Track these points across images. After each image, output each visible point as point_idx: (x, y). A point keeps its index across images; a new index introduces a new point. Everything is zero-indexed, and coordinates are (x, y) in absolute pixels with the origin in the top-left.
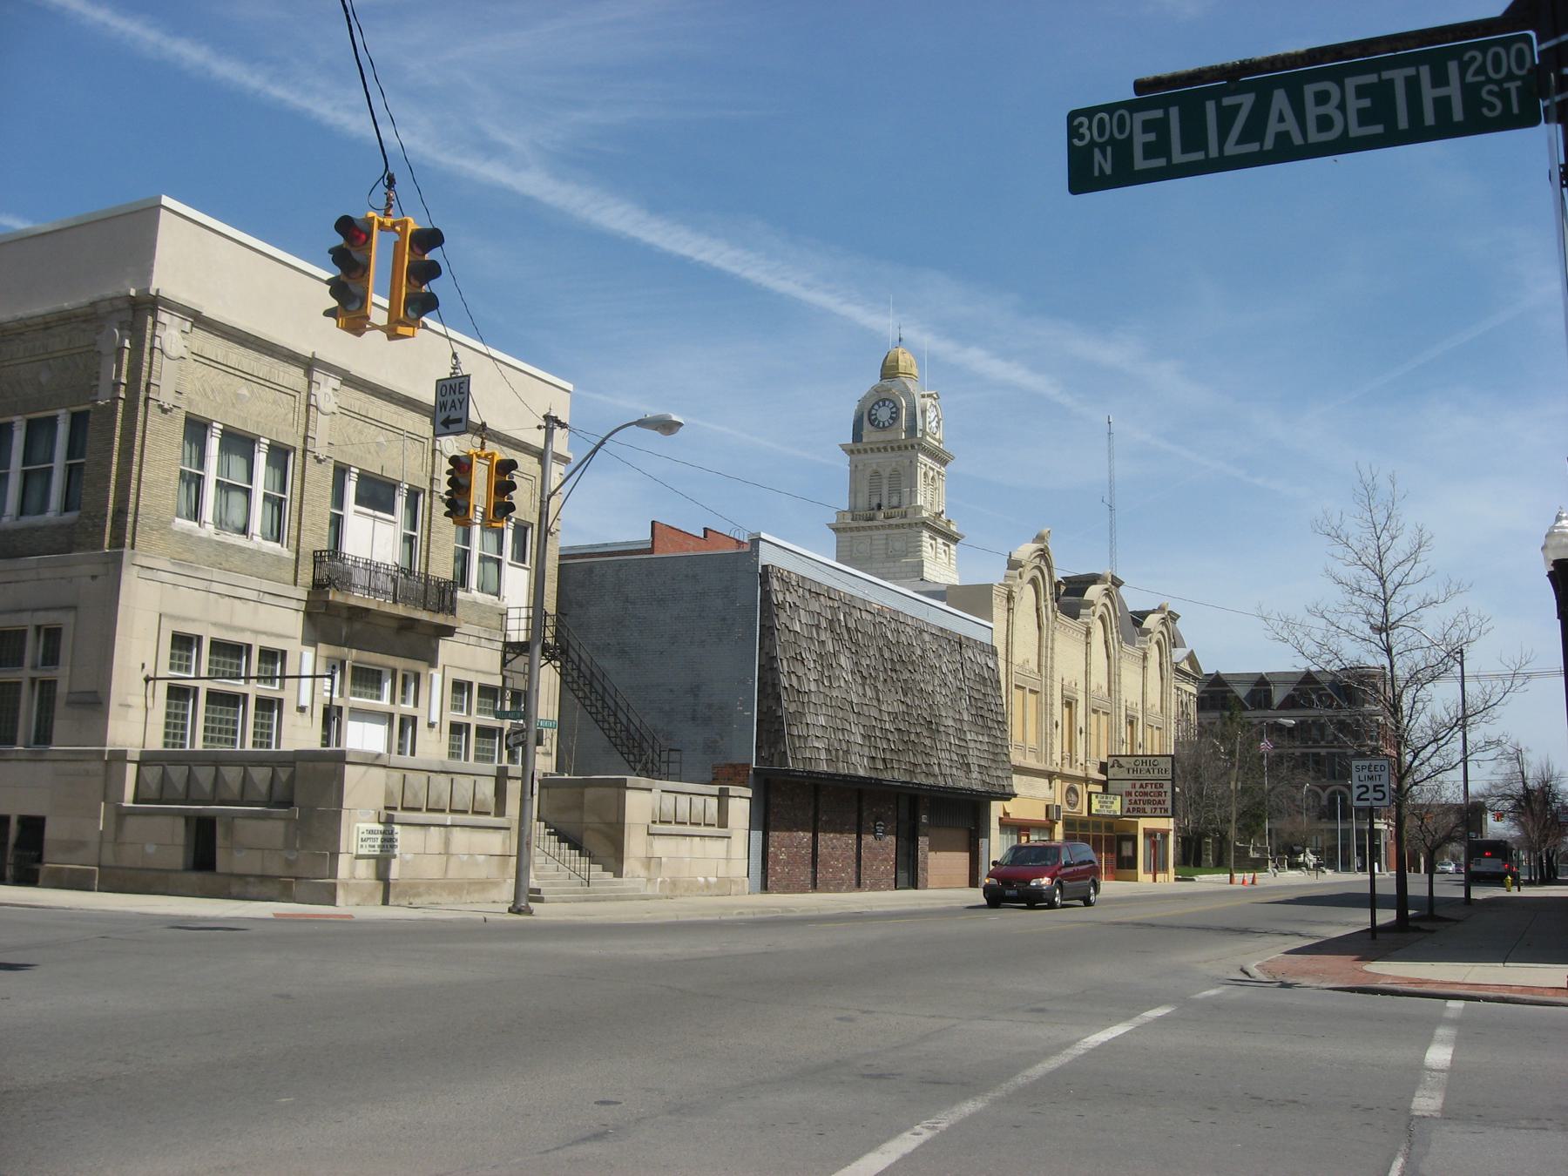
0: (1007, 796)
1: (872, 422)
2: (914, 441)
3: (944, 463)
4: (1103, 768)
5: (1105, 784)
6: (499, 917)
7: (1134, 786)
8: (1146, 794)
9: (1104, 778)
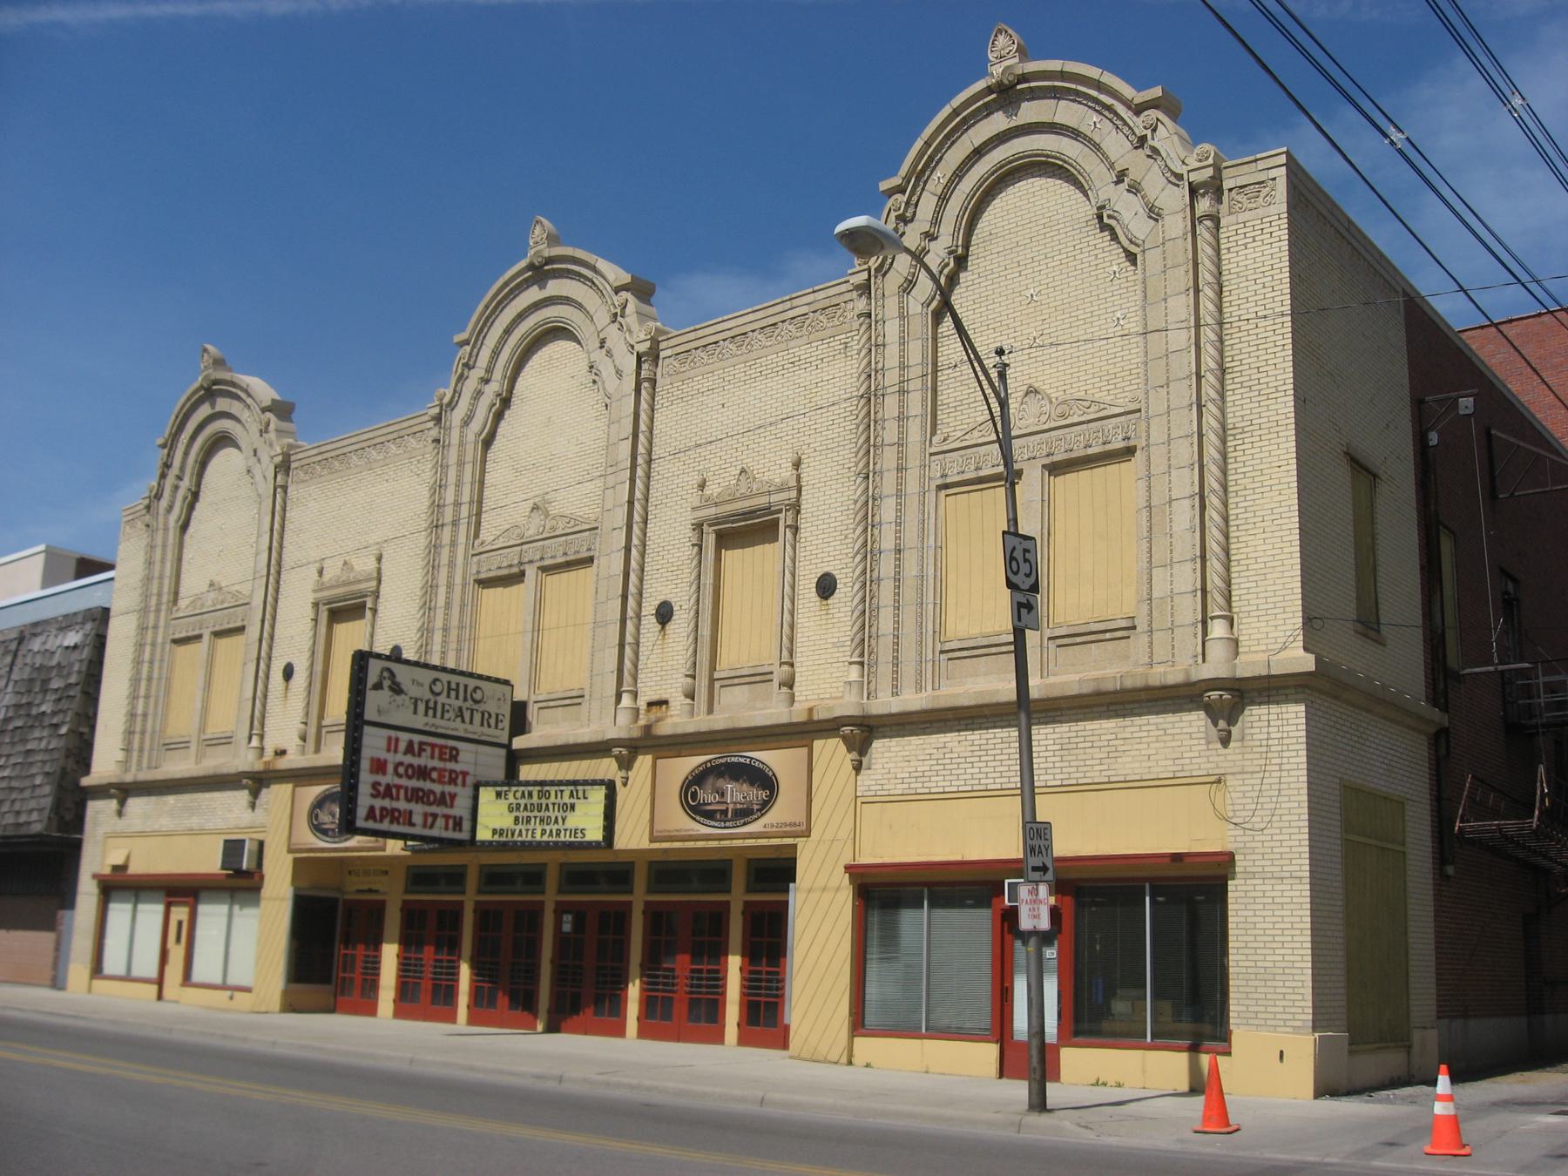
7: (392, 745)
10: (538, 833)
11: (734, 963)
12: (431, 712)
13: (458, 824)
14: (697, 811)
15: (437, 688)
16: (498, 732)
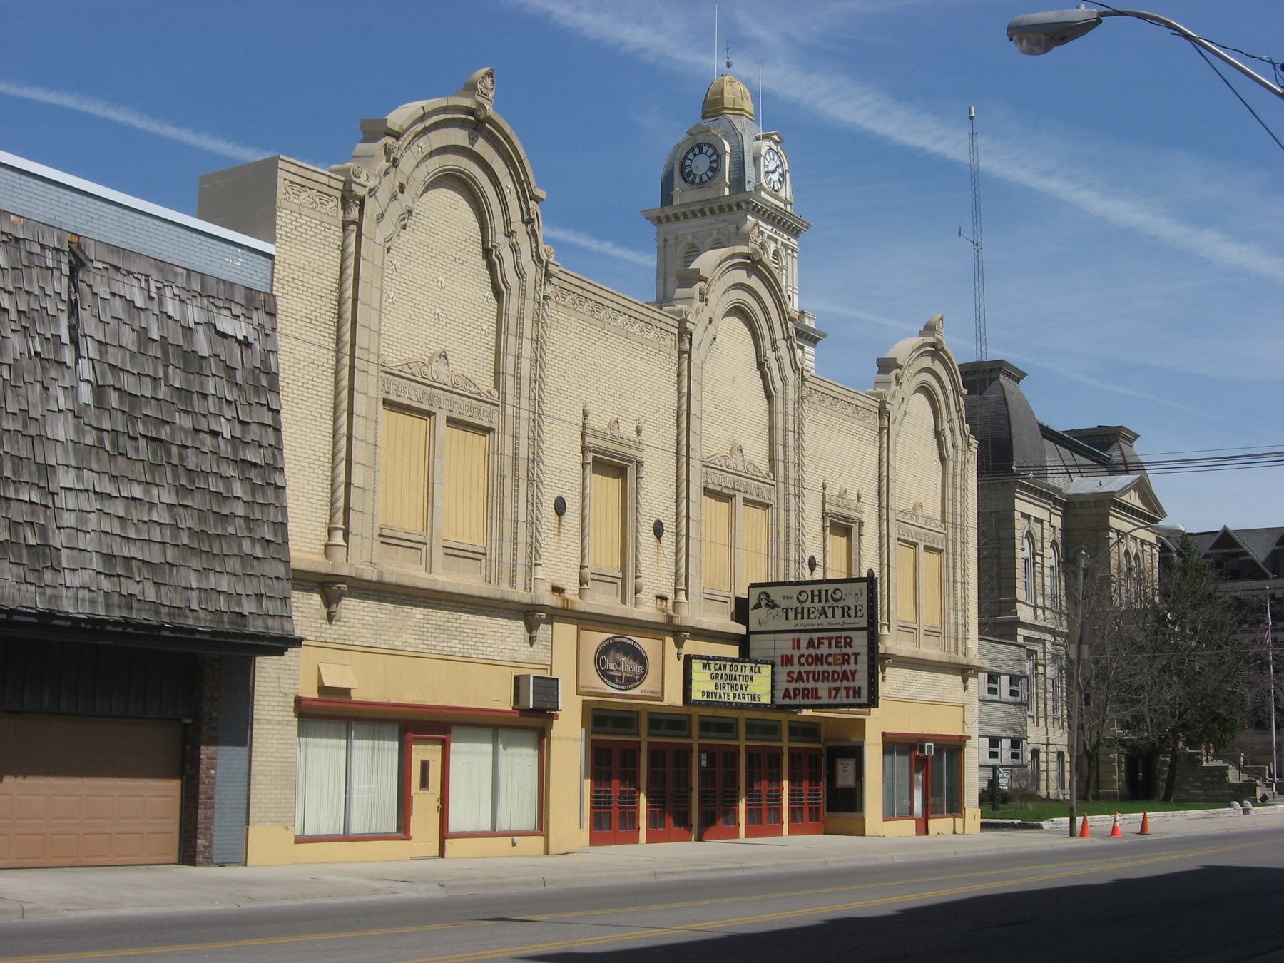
0: (281, 644)
1: (685, 178)
2: (741, 197)
3: (795, 232)
4: (741, 610)
5: (743, 642)
6: (533, 861)
7: (796, 644)
8: (818, 660)
9: (741, 629)
10: (730, 696)
11: (785, 783)
12: (799, 616)
13: (857, 692)
14: (605, 674)
15: (803, 598)
16: (857, 620)
